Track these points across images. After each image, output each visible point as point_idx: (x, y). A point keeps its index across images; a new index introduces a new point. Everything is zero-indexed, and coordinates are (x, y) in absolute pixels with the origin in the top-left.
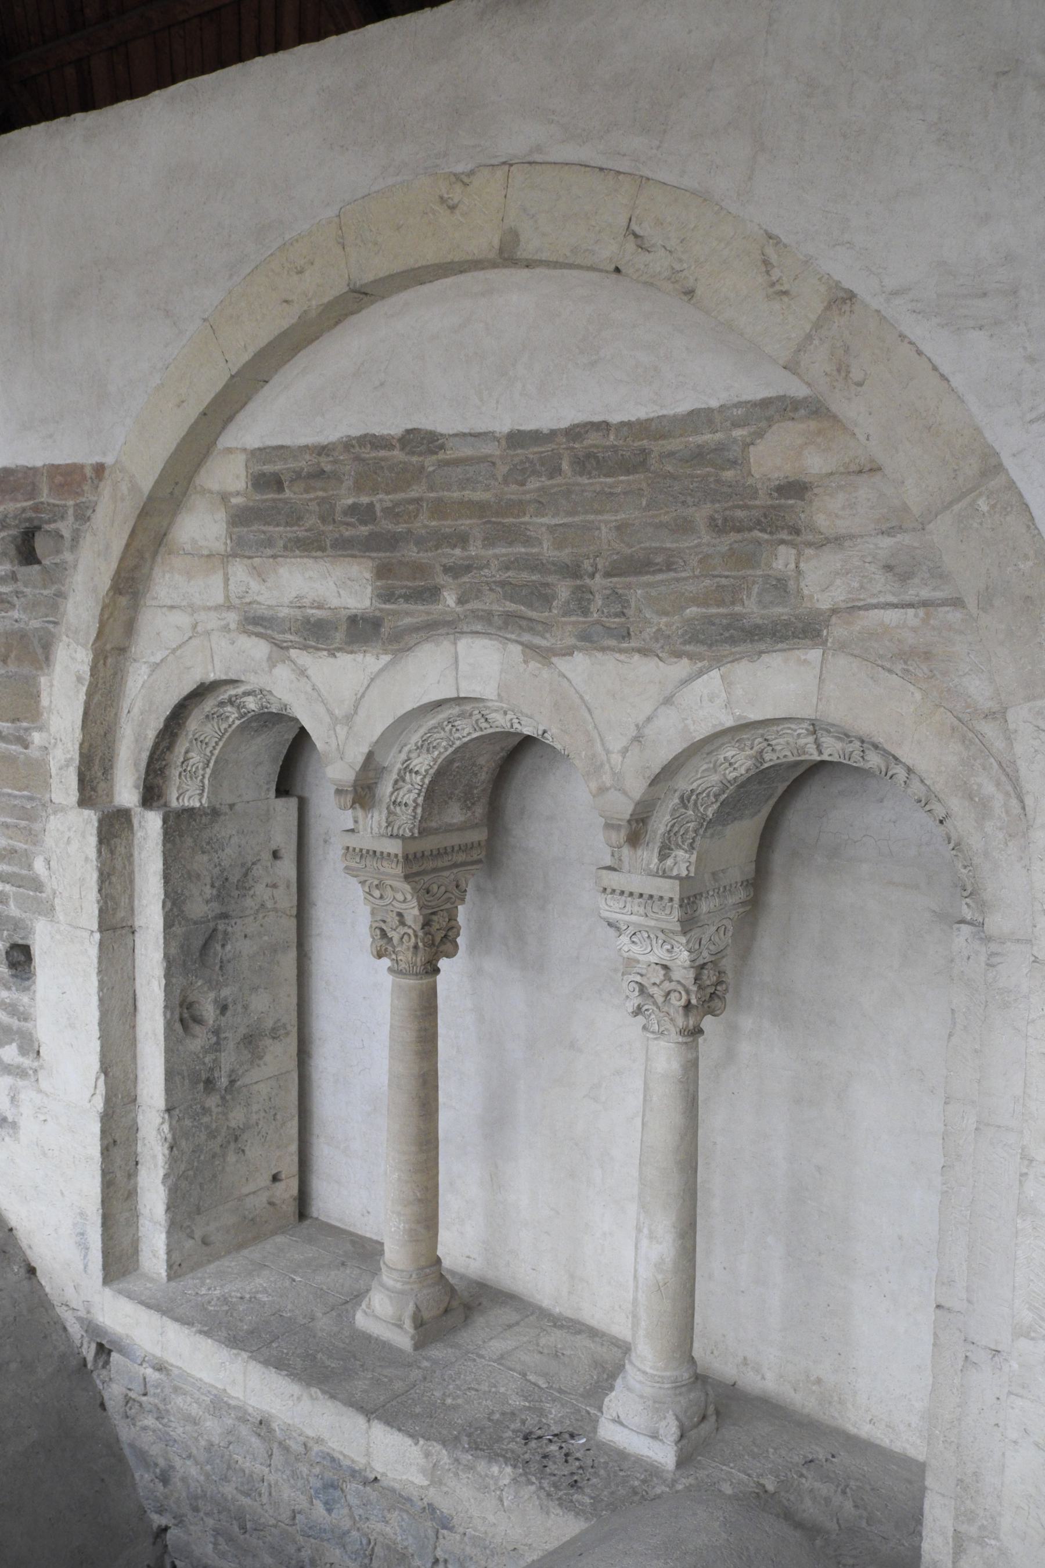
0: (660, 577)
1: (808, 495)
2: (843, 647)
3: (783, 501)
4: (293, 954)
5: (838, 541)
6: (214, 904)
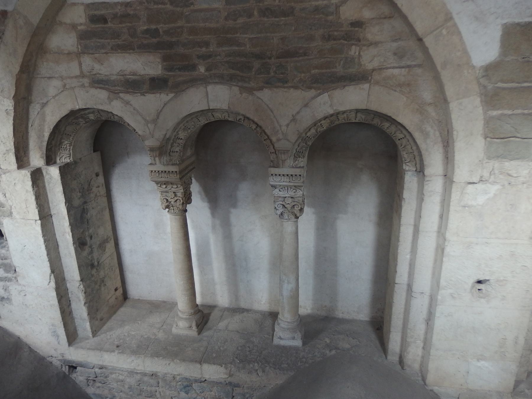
0: (301, 58)
1: (364, 26)
2: (377, 83)
3: (353, 29)
4: (108, 210)
5: (376, 44)
6: (81, 199)
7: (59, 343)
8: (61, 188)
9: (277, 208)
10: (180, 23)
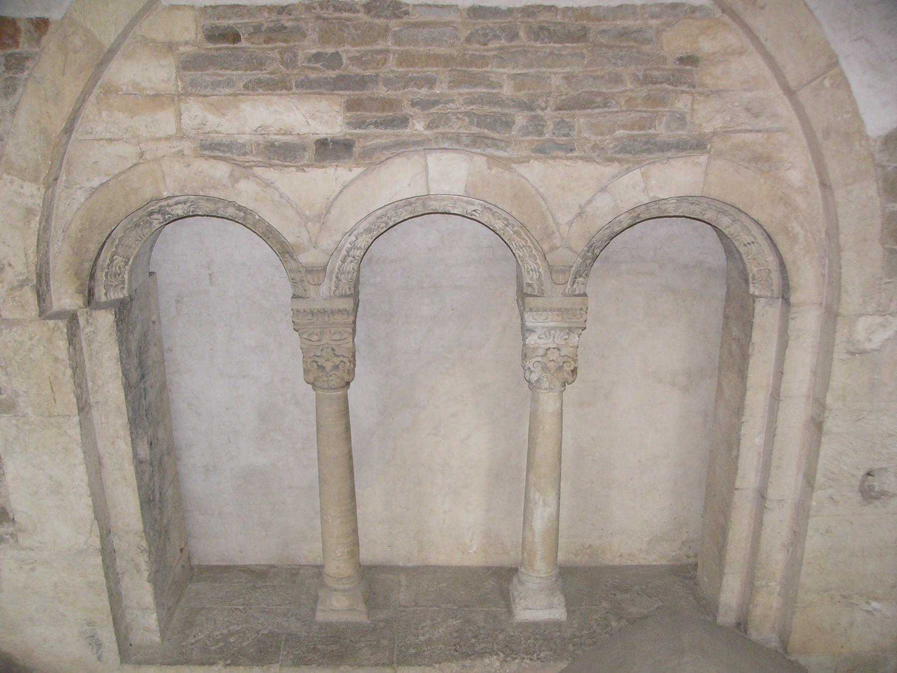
0: (597, 111)
2: (720, 154)
5: (719, 93)
7: (99, 658)
8: (115, 350)
9: (532, 369)
10: (380, 45)
